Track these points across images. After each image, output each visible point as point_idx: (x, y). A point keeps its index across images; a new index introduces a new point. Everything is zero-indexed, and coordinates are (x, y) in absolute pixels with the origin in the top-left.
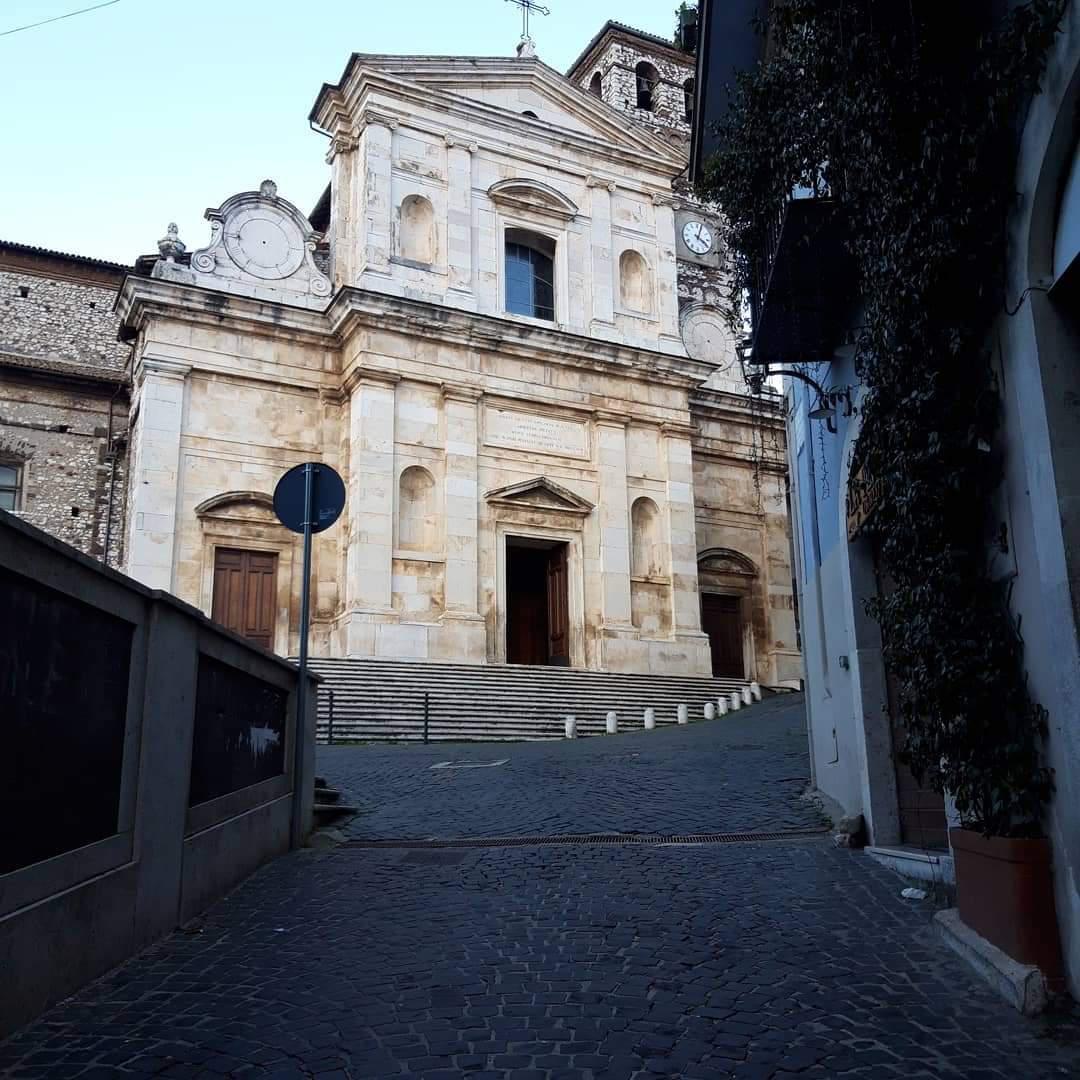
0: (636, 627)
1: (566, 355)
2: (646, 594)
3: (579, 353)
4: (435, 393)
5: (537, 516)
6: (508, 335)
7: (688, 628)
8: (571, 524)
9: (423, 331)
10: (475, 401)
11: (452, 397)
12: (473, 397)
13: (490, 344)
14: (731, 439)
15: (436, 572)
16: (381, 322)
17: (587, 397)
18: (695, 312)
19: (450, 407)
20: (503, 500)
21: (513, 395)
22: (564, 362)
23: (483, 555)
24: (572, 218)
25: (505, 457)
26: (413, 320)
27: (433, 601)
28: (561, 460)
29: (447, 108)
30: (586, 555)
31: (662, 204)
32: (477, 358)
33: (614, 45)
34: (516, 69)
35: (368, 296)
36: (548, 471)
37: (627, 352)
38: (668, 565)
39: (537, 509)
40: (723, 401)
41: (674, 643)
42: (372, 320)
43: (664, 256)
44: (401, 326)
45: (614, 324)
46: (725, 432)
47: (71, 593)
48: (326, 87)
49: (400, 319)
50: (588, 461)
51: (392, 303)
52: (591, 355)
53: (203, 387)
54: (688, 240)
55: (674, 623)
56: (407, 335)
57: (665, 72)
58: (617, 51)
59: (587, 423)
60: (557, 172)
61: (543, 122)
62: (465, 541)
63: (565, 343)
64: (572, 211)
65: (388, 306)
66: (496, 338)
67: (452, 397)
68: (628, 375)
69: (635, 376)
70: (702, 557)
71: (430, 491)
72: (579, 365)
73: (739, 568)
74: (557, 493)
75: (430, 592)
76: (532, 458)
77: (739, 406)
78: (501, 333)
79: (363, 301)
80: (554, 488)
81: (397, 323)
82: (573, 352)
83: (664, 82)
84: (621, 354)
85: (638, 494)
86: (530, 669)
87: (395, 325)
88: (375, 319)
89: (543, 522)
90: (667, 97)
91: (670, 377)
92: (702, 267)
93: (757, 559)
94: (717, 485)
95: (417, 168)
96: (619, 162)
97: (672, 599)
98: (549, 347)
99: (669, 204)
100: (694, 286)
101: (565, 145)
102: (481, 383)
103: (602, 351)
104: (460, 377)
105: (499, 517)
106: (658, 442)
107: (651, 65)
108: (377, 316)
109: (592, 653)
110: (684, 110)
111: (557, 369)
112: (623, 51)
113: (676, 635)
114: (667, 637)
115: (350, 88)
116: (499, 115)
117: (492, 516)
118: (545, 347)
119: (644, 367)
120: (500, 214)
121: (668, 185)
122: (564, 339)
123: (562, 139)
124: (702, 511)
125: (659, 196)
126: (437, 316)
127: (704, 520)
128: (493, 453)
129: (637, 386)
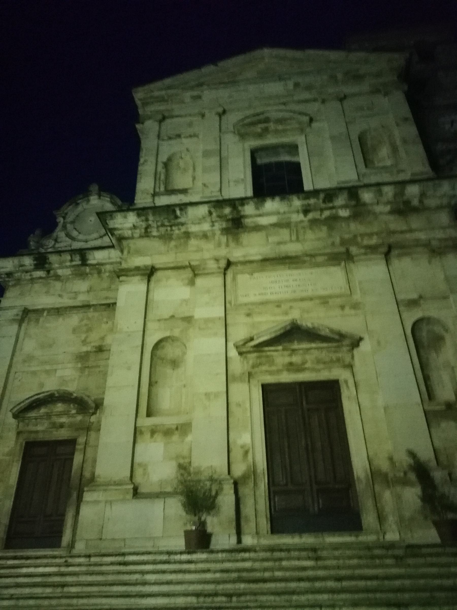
47: (15, 489)
53: (37, 321)
75: (177, 457)
85: (417, 314)
86: (168, 583)
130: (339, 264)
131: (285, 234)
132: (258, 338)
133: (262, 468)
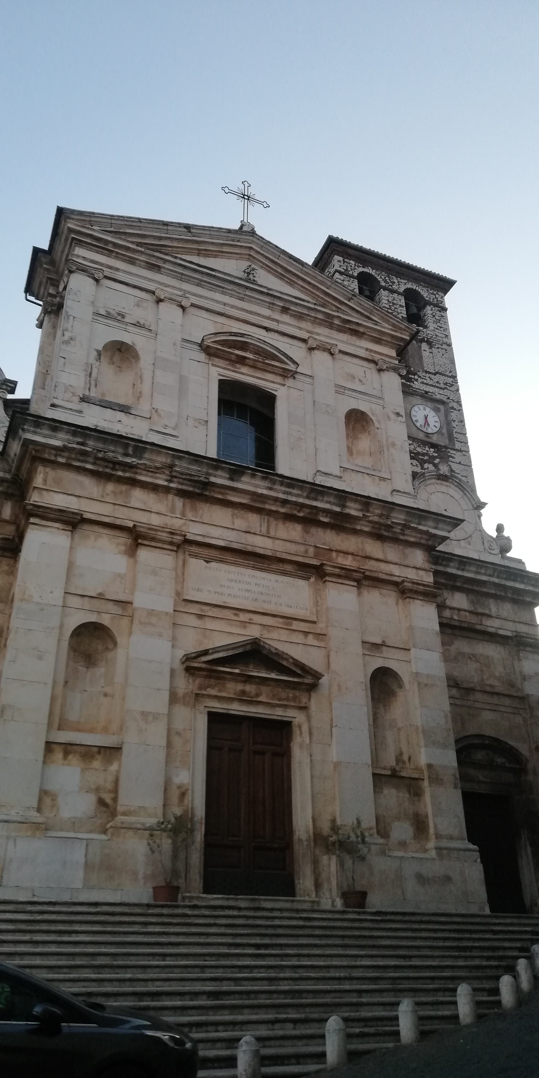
0: (382, 837)
1: (285, 502)
2: (394, 791)
3: (301, 500)
4: (124, 540)
5: (250, 688)
6: (215, 476)
7: (451, 838)
8: (295, 699)
9: (113, 469)
10: (175, 548)
11: (146, 542)
12: (171, 543)
13: (194, 487)
14: (480, 610)
15: (109, 761)
16: (61, 456)
17: (311, 550)
18: (428, 482)
19: (143, 554)
20: (204, 666)
21: (222, 543)
22: (282, 510)
23: (177, 742)
24: (293, 375)
25: (210, 614)
26: (100, 455)
27: (101, 802)
28: (281, 620)
29: (159, 267)
30: (314, 738)
31: (388, 369)
32: (179, 502)
33: (336, 256)
34: (233, 241)
35: (44, 424)
36: (265, 632)
37: (356, 501)
38: (420, 752)
39: (249, 679)
40: (467, 567)
41: (434, 859)
42: (49, 454)
43: (393, 416)
44: (87, 462)
45: (341, 477)
46: (472, 602)
48: (37, 252)
49: (84, 453)
50: (314, 622)
51: (74, 434)
52: (314, 503)
54: (417, 421)
55: (432, 831)
56: (93, 473)
57: (385, 281)
58: (339, 261)
59: (312, 579)
60: (276, 334)
61: (261, 286)
62: (150, 718)
63: (283, 489)
64: (292, 367)
65: (69, 437)
66: (202, 479)
67: (146, 542)
68: (358, 528)
69: (366, 529)
70: (460, 746)
71: (110, 655)
72: (301, 514)
73: (504, 760)
74: (276, 658)
75: (98, 790)
76: (243, 617)
77: (485, 574)
78: (210, 475)
79: (39, 430)
80: (271, 653)
81: (81, 458)
82: (294, 499)
83: (385, 289)
84: (349, 504)
85: (378, 663)
87: (79, 461)
88: (54, 452)
89: (257, 695)
90: (388, 300)
91: (407, 532)
92: (433, 445)
93: (524, 749)
94: (469, 661)
95: (123, 317)
96: (341, 330)
97: (427, 797)
98: (265, 492)
99: (395, 369)
100: (425, 462)
101: (285, 310)
102: (184, 528)
103: (326, 499)
104: (155, 520)
105: (200, 688)
106: (397, 604)
107: (371, 275)
108: (56, 448)
109: (324, 875)
110: (405, 312)
111: (276, 519)
112: (344, 262)
113: (436, 848)
114: (426, 851)
115: (59, 247)
116: (214, 276)
117: (191, 687)
118: (260, 491)
119: (376, 519)
120: (213, 365)
121: (393, 353)
122: (282, 484)
123: (281, 304)
124: (454, 691)
125: (385, 362)
126: (130, 451)
127: (458, 702)
128: (195, 609)
129: (369, 541)
130: (308, 579)
131: (254, 520)
132: (213, 653)
133: (199, 817)
